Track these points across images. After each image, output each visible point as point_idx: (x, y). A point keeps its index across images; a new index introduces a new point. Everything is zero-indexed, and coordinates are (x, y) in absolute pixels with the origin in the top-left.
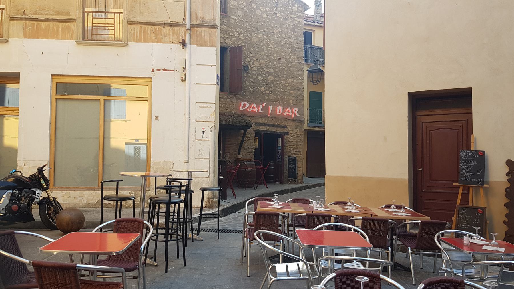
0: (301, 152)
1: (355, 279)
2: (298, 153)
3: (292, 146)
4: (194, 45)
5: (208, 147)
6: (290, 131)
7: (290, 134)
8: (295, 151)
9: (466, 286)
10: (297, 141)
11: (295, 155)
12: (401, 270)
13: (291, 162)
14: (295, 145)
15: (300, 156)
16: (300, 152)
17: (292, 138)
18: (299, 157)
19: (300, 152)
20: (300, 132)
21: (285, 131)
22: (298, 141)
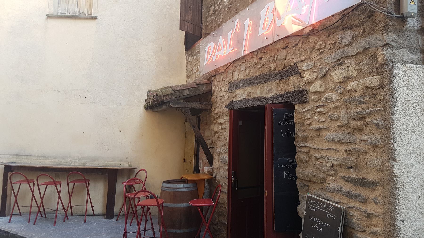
0: (380, 190)
1: (8, 173)
2: (362, 192)
3: (324, 154)
4: (285, 36)
5: (82, 204)
6: (310, 83)
7: (313, 97)
8: (347, 179)
9: (214, 61)
10: (347, 125)
11: (345, 200)
12: (206, 221)
13: (315, 223)
14: (342, 148)
15: (371, 208)
16: (372, 185)
17: (320, 113)
18: (369, 216)
19: (372, 185)
20: (361, 74)
21: (292, 89)
22: (353, 124)
